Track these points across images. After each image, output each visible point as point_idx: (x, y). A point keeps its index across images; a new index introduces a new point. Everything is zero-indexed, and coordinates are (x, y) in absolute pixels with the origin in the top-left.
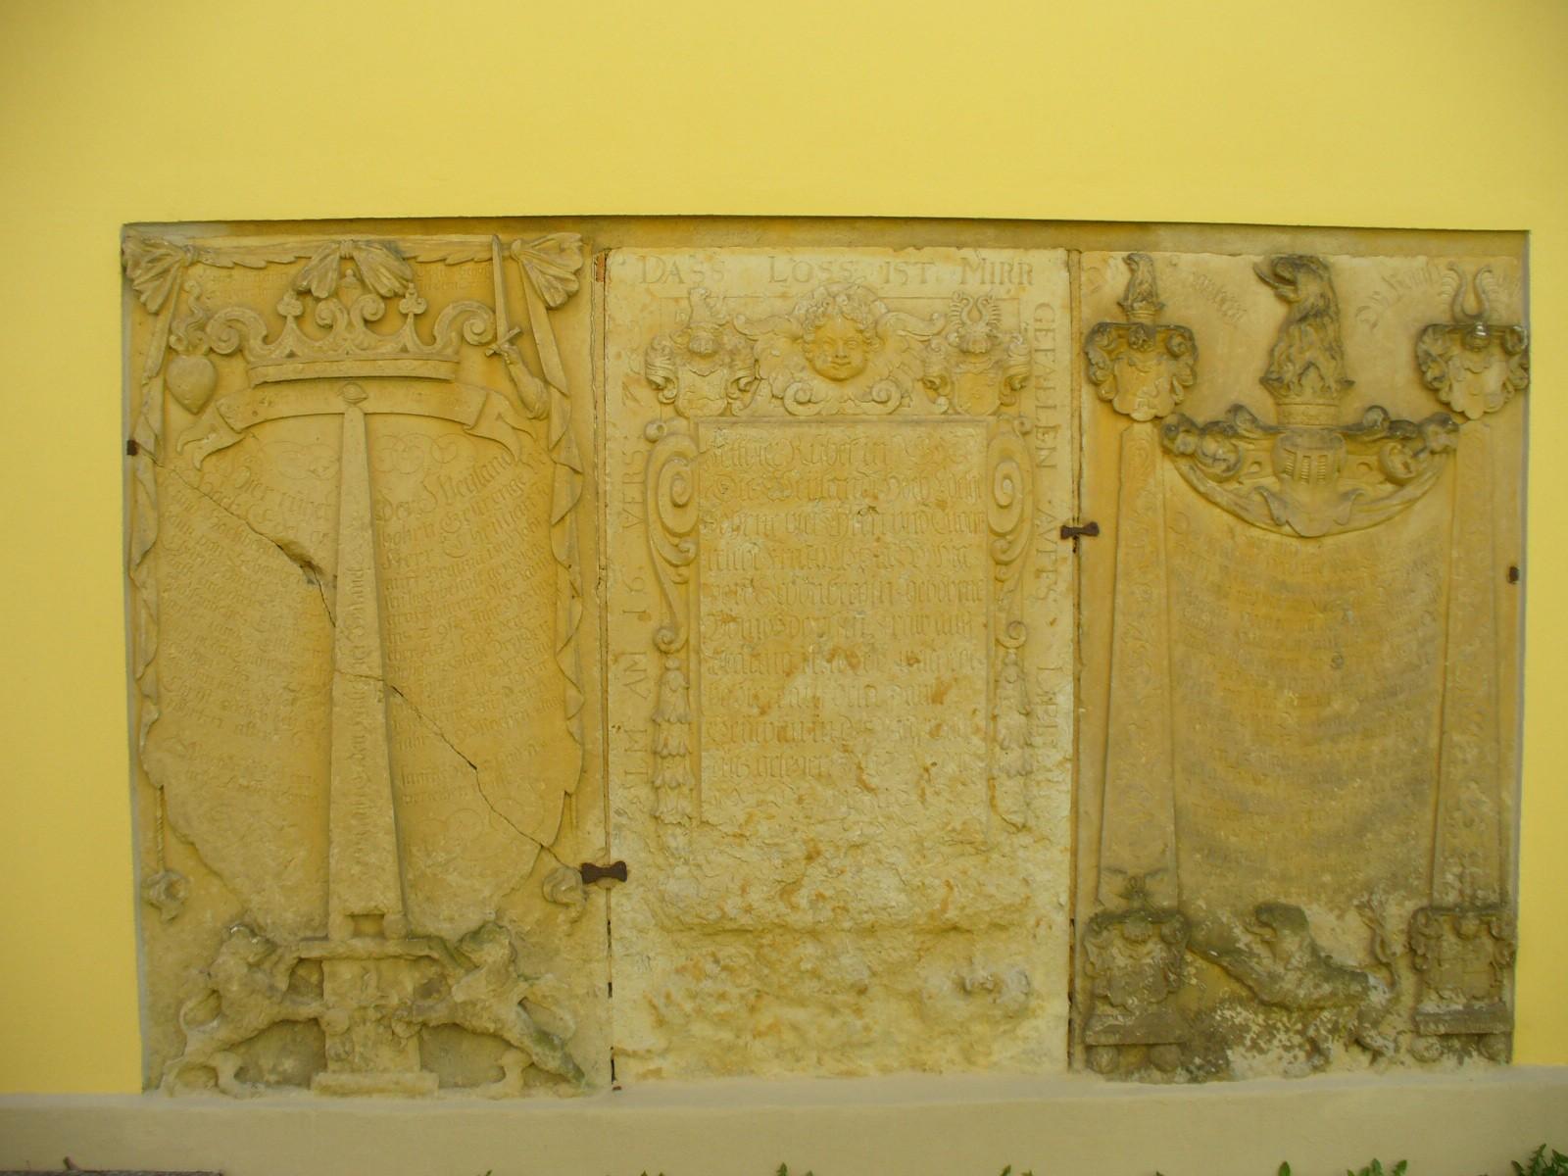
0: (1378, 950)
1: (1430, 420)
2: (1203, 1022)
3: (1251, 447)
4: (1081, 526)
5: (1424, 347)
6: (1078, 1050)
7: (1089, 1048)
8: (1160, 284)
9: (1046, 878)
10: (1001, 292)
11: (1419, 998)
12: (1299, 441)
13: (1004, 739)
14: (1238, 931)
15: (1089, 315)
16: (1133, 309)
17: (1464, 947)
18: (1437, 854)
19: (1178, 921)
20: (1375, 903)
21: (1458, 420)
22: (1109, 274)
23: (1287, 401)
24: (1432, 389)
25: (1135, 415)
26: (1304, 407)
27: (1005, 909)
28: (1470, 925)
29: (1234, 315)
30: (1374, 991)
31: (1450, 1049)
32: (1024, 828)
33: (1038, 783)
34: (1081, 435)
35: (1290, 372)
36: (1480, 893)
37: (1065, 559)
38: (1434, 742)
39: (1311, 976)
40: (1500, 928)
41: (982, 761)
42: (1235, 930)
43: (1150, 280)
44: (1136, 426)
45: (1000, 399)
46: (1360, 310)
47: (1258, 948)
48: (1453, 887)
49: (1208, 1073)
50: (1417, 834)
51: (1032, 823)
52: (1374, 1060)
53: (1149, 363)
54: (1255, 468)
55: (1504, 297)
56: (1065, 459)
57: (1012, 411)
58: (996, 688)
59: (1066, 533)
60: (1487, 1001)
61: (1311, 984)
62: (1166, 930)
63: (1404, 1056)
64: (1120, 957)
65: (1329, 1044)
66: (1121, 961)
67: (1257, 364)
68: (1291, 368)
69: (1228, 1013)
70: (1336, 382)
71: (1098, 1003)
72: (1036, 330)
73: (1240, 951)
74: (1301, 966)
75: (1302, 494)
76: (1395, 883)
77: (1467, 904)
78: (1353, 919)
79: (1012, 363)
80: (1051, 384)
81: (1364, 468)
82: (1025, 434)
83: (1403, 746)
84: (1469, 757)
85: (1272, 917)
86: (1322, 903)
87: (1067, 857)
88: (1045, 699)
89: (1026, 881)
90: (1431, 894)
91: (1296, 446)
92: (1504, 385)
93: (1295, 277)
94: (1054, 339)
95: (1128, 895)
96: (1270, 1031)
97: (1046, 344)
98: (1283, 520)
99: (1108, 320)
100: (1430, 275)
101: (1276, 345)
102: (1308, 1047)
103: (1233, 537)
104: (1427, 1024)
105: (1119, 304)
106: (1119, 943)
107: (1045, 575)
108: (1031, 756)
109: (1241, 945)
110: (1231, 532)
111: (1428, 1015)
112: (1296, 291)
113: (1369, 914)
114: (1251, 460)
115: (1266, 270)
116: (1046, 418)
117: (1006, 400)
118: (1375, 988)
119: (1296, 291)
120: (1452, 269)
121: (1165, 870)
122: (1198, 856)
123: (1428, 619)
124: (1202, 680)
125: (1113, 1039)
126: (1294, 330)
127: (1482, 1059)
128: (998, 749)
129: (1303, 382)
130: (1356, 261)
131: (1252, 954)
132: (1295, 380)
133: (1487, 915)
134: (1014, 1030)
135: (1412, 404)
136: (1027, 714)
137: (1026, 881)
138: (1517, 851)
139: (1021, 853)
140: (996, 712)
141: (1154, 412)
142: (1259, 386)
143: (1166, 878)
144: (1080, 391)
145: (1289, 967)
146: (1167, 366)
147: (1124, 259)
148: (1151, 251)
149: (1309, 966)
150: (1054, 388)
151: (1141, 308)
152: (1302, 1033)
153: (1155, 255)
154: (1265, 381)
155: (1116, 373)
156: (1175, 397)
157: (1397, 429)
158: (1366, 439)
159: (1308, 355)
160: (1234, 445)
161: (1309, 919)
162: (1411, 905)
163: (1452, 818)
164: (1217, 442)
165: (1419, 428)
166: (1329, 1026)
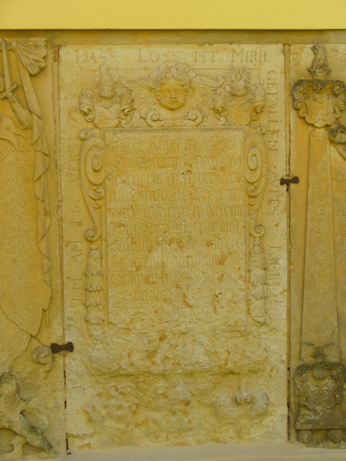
4: (290, 178)
9: (276, 348)
13: (254, 281)
15: (294, 76)
22: (304, 56)
25: (316, 125)
33: (271, 302)
34: (290, 135)
41: (243, 292)
44: (317, 130)
45: (251, 117)
51: (268, 321)
56: (282, 146)
57: (256, 123)
59: (283, 182)
62: (334, 373)
64: (312, 386)
71: (302, 409)
72: (268, 84)
79: (256, 100)
80: (275, 110)
82: (263, 134)
87: (285, 338)
88: (274, 261)
89: (265, 350)
97: (273, 90)
99: (303, 79)
105: (309, 70)
106: (311, 379)
107: (273, 202)
116: (273, 127)
117: (254, 118)
121: (333, 344)
125: (309, 427)
128: (251, 286)
136: (265, 269)
137: (265, 350)
139: (263, 336)
140: (250, 268)
141: (325, 123)
143: (333, 348)
144: (289, 113)
146: (332, 101)
150: (277, 112)
151: (319, 72)
153: (327, 46)
155: (307, 104)
156: (336, 116)
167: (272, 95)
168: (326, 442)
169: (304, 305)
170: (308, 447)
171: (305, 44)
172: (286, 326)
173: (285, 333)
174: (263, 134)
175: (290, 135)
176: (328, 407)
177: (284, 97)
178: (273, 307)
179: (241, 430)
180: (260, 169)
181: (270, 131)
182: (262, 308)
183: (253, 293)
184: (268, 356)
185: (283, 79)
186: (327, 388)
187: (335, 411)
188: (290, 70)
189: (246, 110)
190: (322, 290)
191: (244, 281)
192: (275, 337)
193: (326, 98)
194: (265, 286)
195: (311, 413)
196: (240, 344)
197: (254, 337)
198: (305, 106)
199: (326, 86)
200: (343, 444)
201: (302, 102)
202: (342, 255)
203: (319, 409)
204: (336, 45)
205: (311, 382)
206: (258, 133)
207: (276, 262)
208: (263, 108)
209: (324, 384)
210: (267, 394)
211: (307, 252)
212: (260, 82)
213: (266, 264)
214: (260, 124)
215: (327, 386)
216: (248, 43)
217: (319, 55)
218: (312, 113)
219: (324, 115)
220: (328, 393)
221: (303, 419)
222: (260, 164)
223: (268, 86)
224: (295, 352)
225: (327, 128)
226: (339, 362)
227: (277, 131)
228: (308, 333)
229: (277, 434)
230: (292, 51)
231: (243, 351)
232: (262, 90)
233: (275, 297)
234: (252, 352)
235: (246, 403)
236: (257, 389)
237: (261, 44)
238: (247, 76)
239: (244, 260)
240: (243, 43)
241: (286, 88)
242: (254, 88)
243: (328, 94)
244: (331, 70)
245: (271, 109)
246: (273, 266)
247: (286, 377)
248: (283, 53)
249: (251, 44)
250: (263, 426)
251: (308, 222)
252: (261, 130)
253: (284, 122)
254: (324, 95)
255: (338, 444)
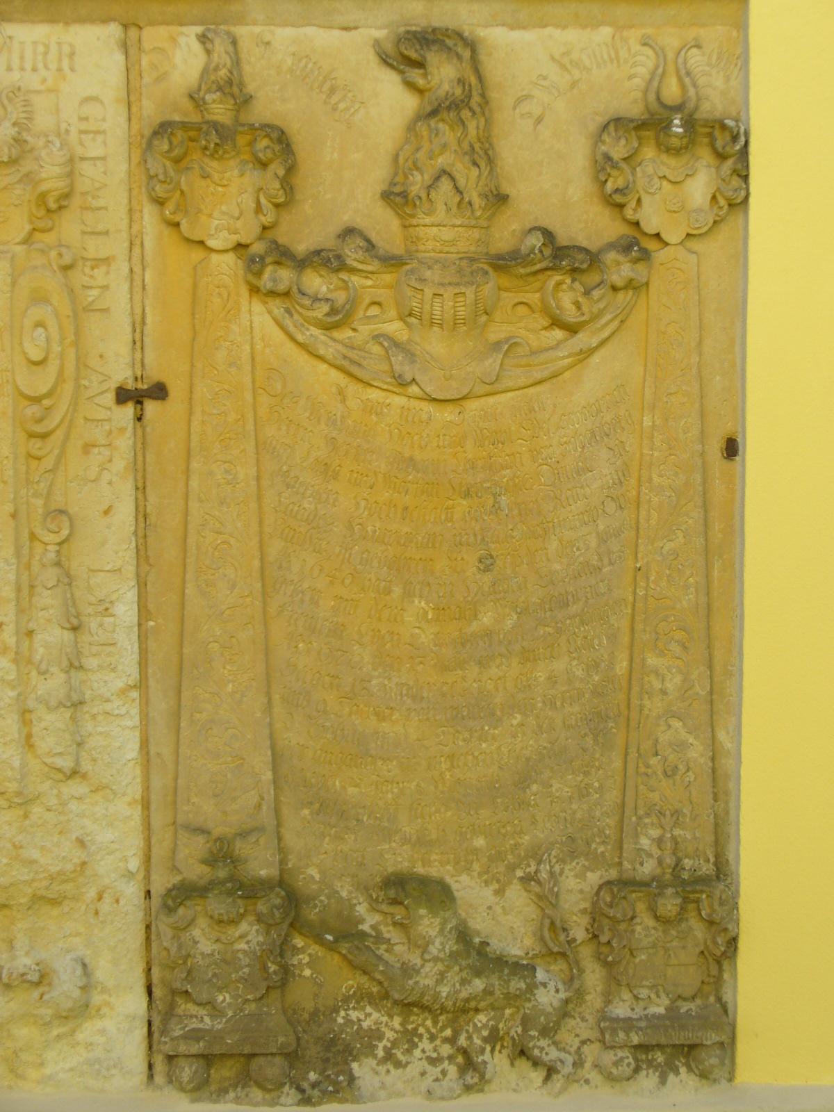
0: (547, 935)
1: (612, 246)
2: (320, 1026)
3: (369, 283)
4: (145, 387)
5: (604, 148)
6: (160, 1066)
7: (170, 1058)
8: (247, 69)
9: (111, 839)
10: (33, 81)
11: (608, 999)
12: (428, 274)
13: (41, 662)
14: (362, 909)
15: (150, 110)
16: (205, 103)
17: (665, 932)
18: (628, 812)
19: (278, 895)
20: (544, 875)
21: (651, 245)
22: (178, 57)
23: (414, 222)
24: (615, 203)
25: (211, 243)
26: (435, 229)
27: (52, 878)
28: (669, 904)
29: (347, 109)
30: (542, 989)
31: (650, 1064)
32: (74, 773)
33: (94, 717)
34: (144, 269)
35: (417, 182)
36: (687, 863)
37: (122, 430)
38: (621, 667)
39: (457, 968)
40: (711, 906)
41: (13, 688)
42: (358, 908)
43: (229, 64)
44: (215, 258)
45: (31, 222)
46: (520, 100)
47: (389, 932)
48: (650, 855)
49: (324, 1092)
50: (601, 787)
51: (86, 766)
52: (548, 1078)
53: (228, 174)
54: (374, 311)
55: (719, 82)
56: (119, 299)
57: (50, 238)
58: (31, 595)
59: (123, 396)
60: (699, 1001)
61: (457, 978)
62: (262, 907)
63: (594, 1076)
64: (204, 941)
65: (487, 1056)
66: (206, 946)
67: (378, 176)
68: (418, 177)
69: (354, 1015)
70: (480, 195)
71: (180, 1001)
72: (82, 132)
73: (363, 935)
74: (442, 955)
75: (435, 344)
76: (573, 849)
77: (668, 876)
78: (516, 895)
79: (44, 175)
80: (101, 203)
81: (522, 310)
82: (66, 268)
83: (579, 673)
84: (669, 686)
85: (406, 890)
86: (475, 874)
87: (137, 813)
88: (101, 608)
89: (81, 843)
90: (620, 864)
91: (422, 280)
92: (714, 197)
93: (424, 58)
94: (105, 143)
95: (211, 860)
96: (410, 1038)
97: (95, 150)
98: (408, 377)
99: (177, 118)
100: (617, 53)
101: (401, 149)
102: (460, 1059)
103: (344, 401)
104: (614, 1032)
105: (191, 97)
106: (202, 922)
107: (96, 450)
108: (84, 682)
109: (365, 927)
110: (341, 392)
111: (617, 1020)
112: (425, 75)
113: (537, 889)
114: (367, 301)
115: (389, 47)
116: (95, 248)
117: (41, 224)
118: (544, 985)
119: (425, 75)
120: (645, 45)
121: (260, 829)
122: (306, 812)
123: (611, 507)
124: (306, 585)
125: (196, 1048)
126: (422, 128)
127: (693, 1077)
128: (34, 673)
129: (433, 194)
130: (516, 35)
131: (379, 938)
132: (423, 195)
133: (695, 892)
134: (73, 1032)
135: (586, 223)
136: (75, 629)
137: (81, 843)
138: (738, 808)
139: (73, 806)
140: (31, 626)
141: (235, 238)
142: (380, 203)
143: (262, 841)
144: (141, 211)
145: (427, 957)
146: (252, 178)
147: (197, 35)
148: (235, 25)
149: (454, 956)
150: (106, 208)
151: (214, 101)
152: (452, 1041)
153: (242, 31)
154: (387, 196)
155: (184, 187)
156: (263, 218)
157: (562, 256)
158: (522, 271)
159: (441, 161)
160: (344, 281)
161: (456, 894)
162: (594, 878)
163: (648, 766)
164: (321, 276)
165: (595, 259)
166: (485, 1033)
167: (92, 162)
168: (243, 1088)
169: (182, 725)
170: (193, 1101)
171: (181, 25)
172: (139, 780)
173: (134, 799)
174: (66, 268)
175: (144, 269)
176: (249, 997)
177: (124, 167)
178: (100, 729)
179: (17, 1056)
180: (57, 362)
181: (87, 260)
182: (64, 731)
183: (39, 693)
184: (86, 860)
185: (123, 119)
186: (245, 947)
187: (268, 1006)
188: (141, 94)
189: (16, 203)
190: (230, 686)
191: (15, 661)
192: (106, 809)
193: (236, 172)
194: (73, 673)
195: (205, 1012)
196: (7, 828)
197: (48, 810)
198: (179, 192)
199: (234, 140)
200: (288, 1094)
201: (168, 180)
202: (285, 594)
203: (224, 1000)
204: (267, 28)
205: (203, 930)
206: (51, 265)
207: (107, 609)
208: (67, 196)
209: (237, 935)
210: (87, 961)
211: (188, 585)
212: (59, 127)
213: (78, 616)
214: (60, 241)
215: (245, 940)
216: (22, 21)
217: (216, 55)
218: (199, 211)
219: (232, 217)
220: (247, 960)
221: (180, 1026)
222: (56, 348)
223: (80, 139)
224: (159, 851)
225: (243, 251)
226: (277, 878)
227: (107, 261)
228: (194, 800)
229: (115, 1066)
230: (146, 45)
231: (14, 845)
232: (61, 149)
233: (105, 704)
234: (42, 848)
235: (26, 985)
236: (60, 945)
237: (61, 25)
238: (25, 109)
239: (14, 603)
240: (10, 20)
241: (130, 144)
242: (41, 142)
243: (241, 161)
244: (251, 97)
245: (90, 199)
246: (99, 619)
247: (141, 915)
248: (123, 50)
249: (33, 22)
250: (78, 1044)
251: (190, 503)
252: (60, 255)
253: (125, 235)
254: (232, 163)
255: (274, 1094)
